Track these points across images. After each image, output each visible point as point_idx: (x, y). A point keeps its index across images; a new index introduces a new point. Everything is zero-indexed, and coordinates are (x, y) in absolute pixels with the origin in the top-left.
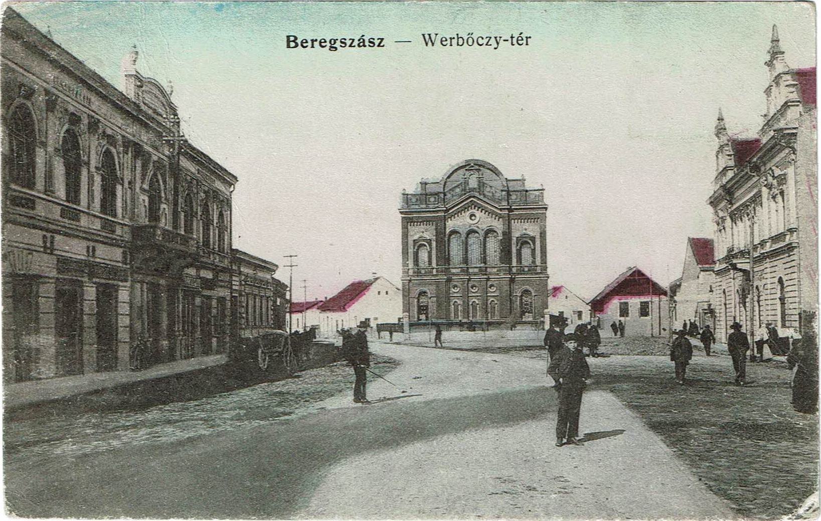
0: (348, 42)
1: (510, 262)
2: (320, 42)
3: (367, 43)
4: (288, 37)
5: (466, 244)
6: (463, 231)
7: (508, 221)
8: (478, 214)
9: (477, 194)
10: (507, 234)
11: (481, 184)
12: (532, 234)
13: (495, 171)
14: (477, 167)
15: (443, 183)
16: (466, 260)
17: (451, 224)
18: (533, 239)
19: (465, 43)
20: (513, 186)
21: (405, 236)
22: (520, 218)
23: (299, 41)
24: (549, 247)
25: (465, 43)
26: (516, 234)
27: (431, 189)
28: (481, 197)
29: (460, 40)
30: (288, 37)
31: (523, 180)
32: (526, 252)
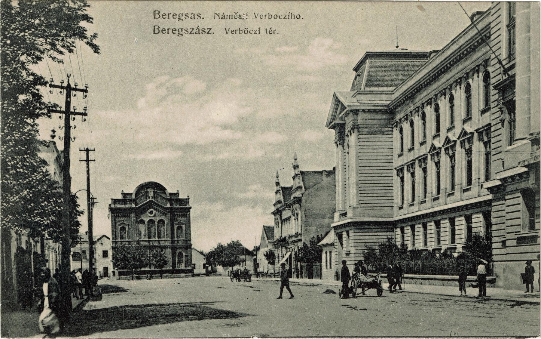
0: (170, 31)
2: (173, 16)
3: (201, 31)
4: (154, 26)
23: (160, 29)
30: (154, 26)
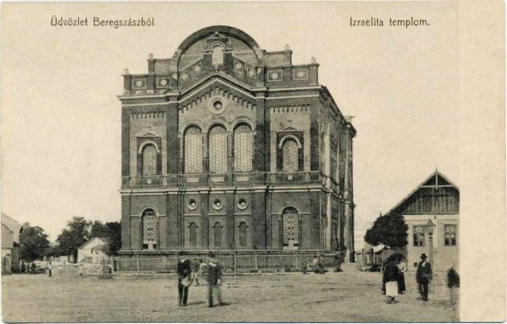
1: (266, 168)
5: (232, 142)
6: (205, 123)
7: (266, 106)
8: (224, 100)
9: (222, 74)
10: (264, 128)
11: (229, 61)
12: (299, 129)
13: (247, 41)
14: (223, 36)
15: (177, 59)
16: (206, 165)
17: (186, 116)
18: (300, 135)
19: (146, 24)
20: (269, 62)
21: (126, 132)
22: (279, 105)
24: (119, 157)
25: (146, 24)
26: (274, 127)
27: (161, 69)
28: (229, 77)
29: (143, 23)
30: (94, 18)
31: (289, 54)
32: (292, 150)
